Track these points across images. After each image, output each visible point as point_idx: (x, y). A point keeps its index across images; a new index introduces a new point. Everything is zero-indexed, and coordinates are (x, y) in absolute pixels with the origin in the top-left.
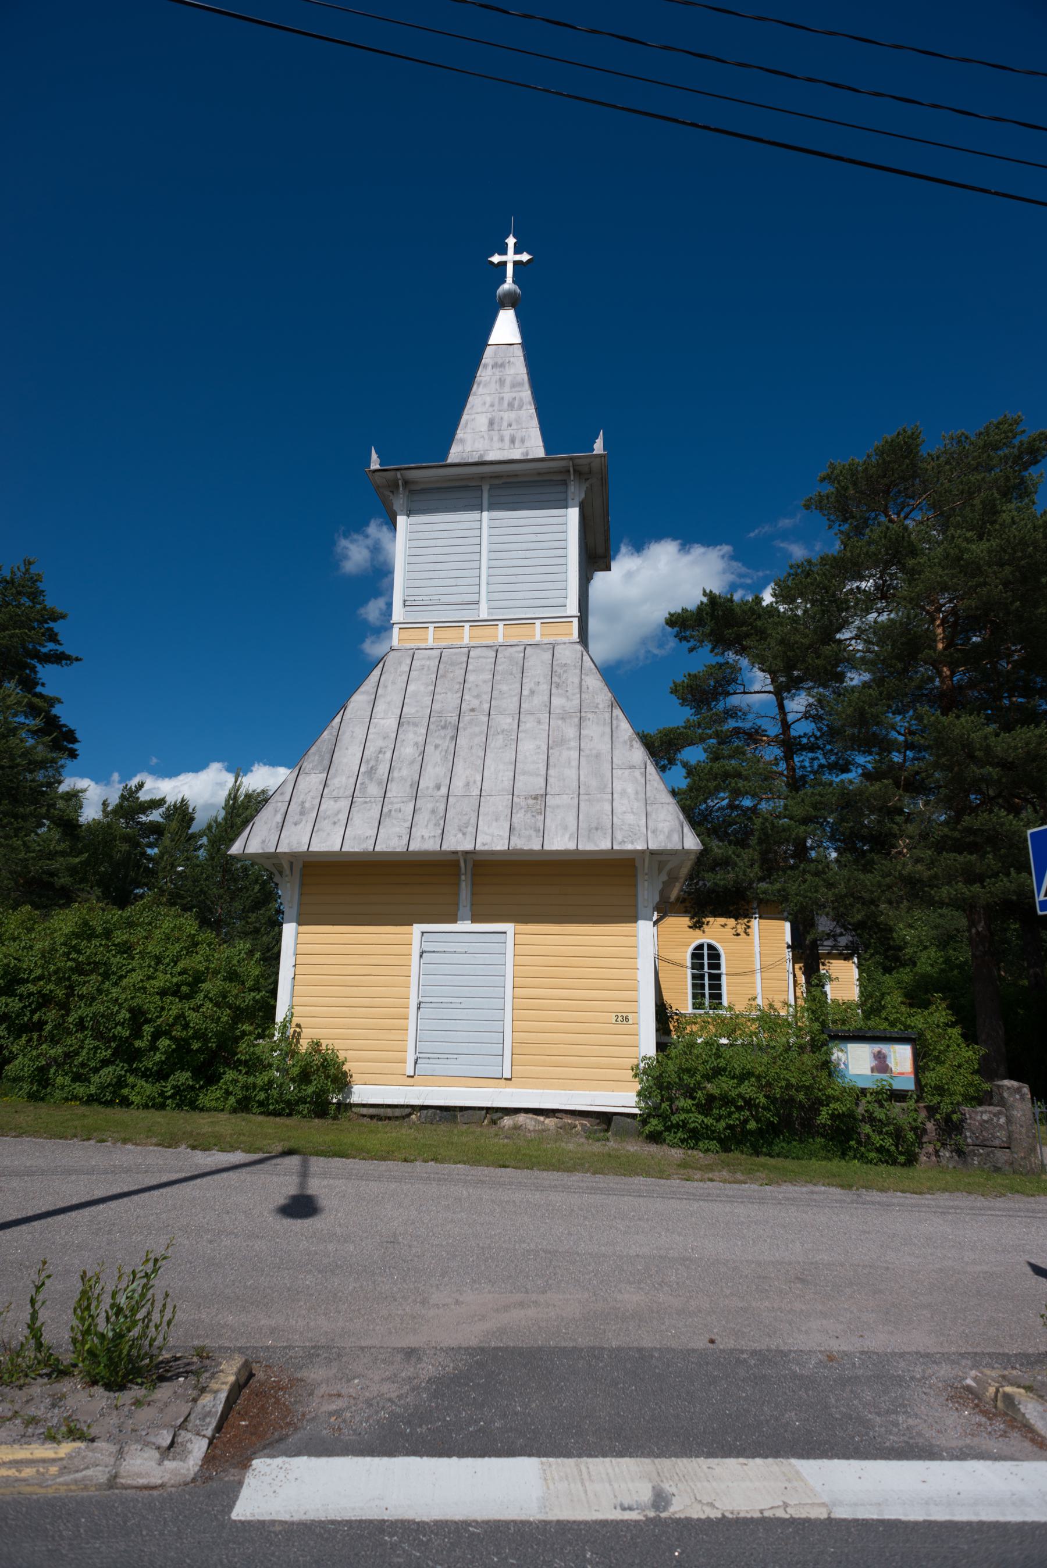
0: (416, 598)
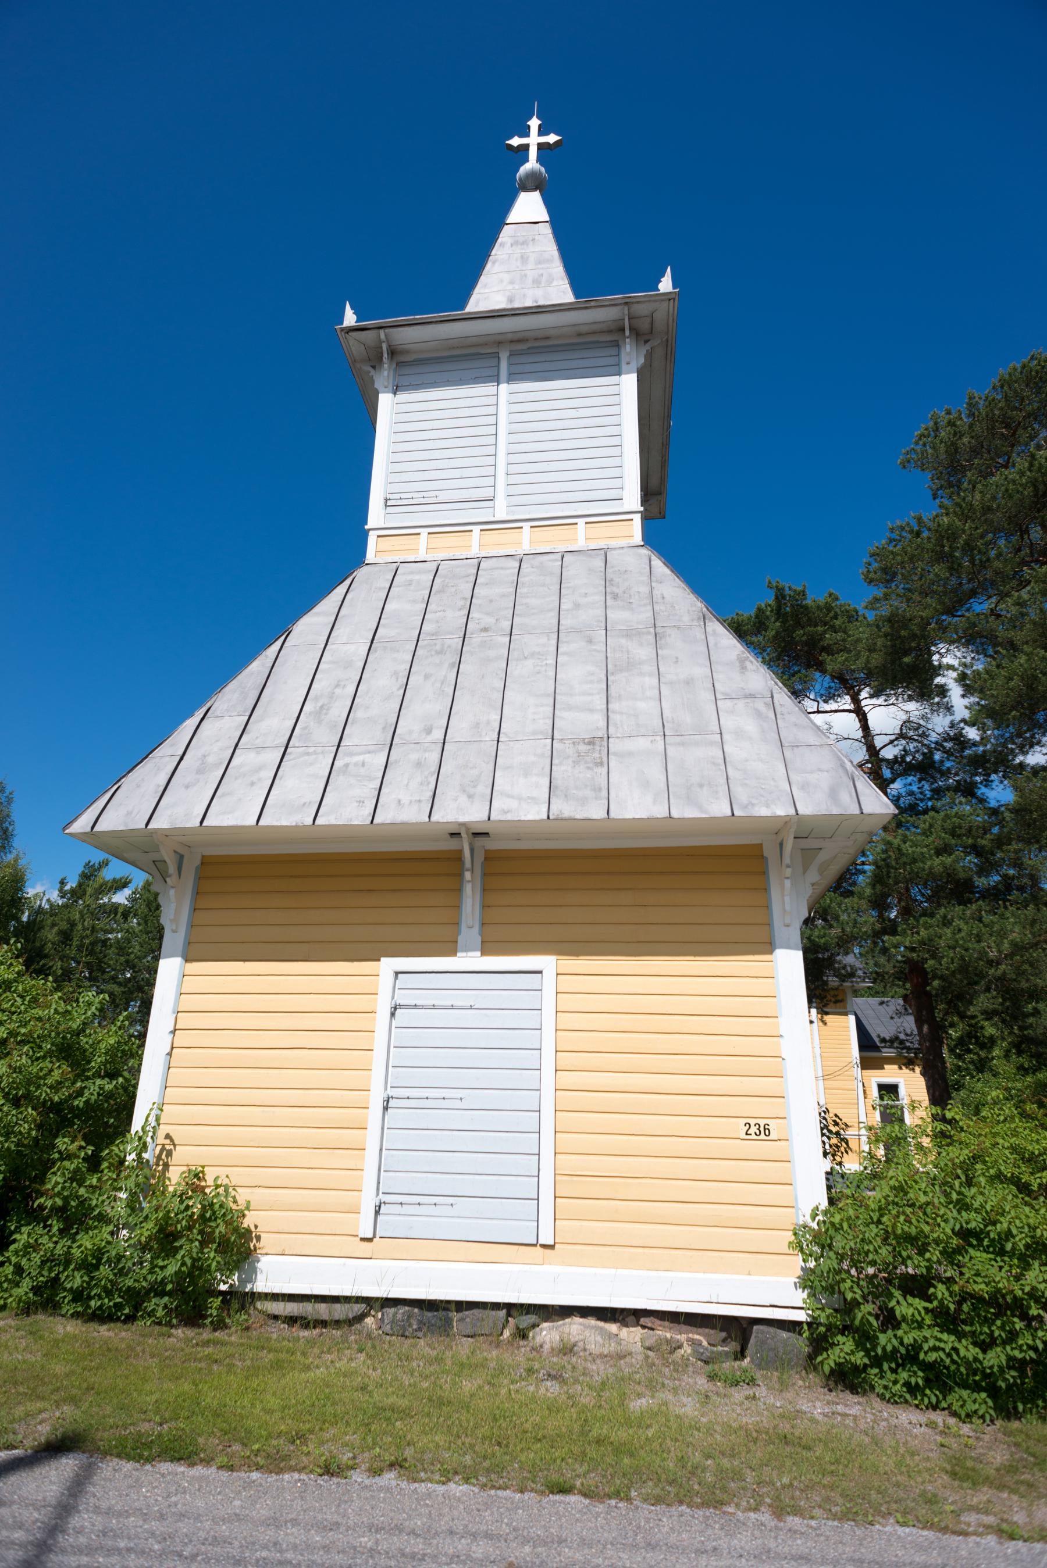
0: (403, 496)
